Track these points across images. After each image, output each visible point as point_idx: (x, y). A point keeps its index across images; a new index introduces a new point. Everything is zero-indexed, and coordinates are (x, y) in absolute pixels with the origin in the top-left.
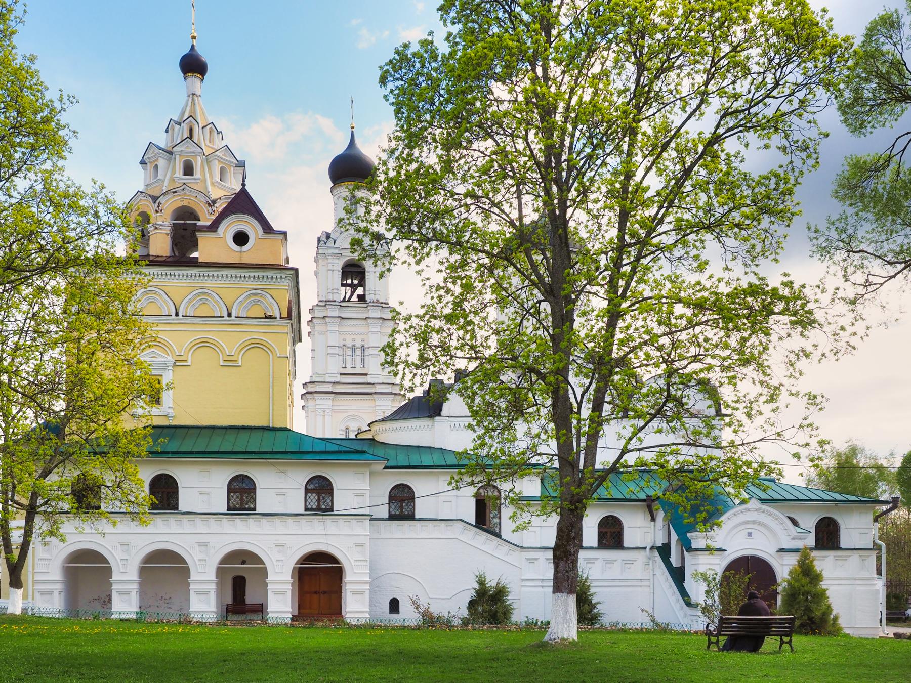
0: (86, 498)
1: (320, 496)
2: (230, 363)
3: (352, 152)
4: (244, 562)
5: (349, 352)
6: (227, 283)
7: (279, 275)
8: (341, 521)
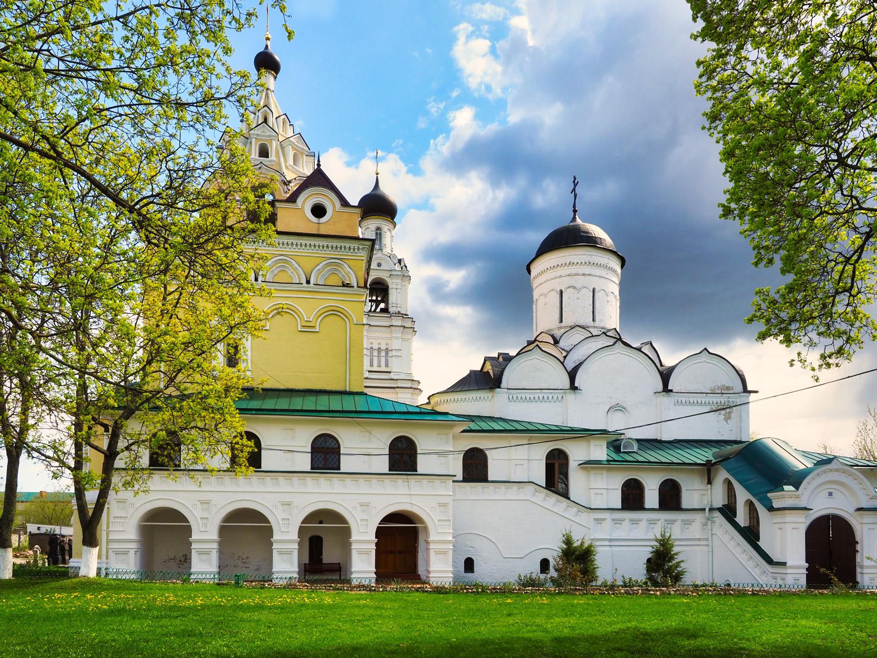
0: (165, 457)
1: (403, 458)
2: (308, 329)
3: (377, 192)
4: (321, 522)
5: (375, 353)
6: (305, 252)
7: (356, 246)
8: (425, 481)
